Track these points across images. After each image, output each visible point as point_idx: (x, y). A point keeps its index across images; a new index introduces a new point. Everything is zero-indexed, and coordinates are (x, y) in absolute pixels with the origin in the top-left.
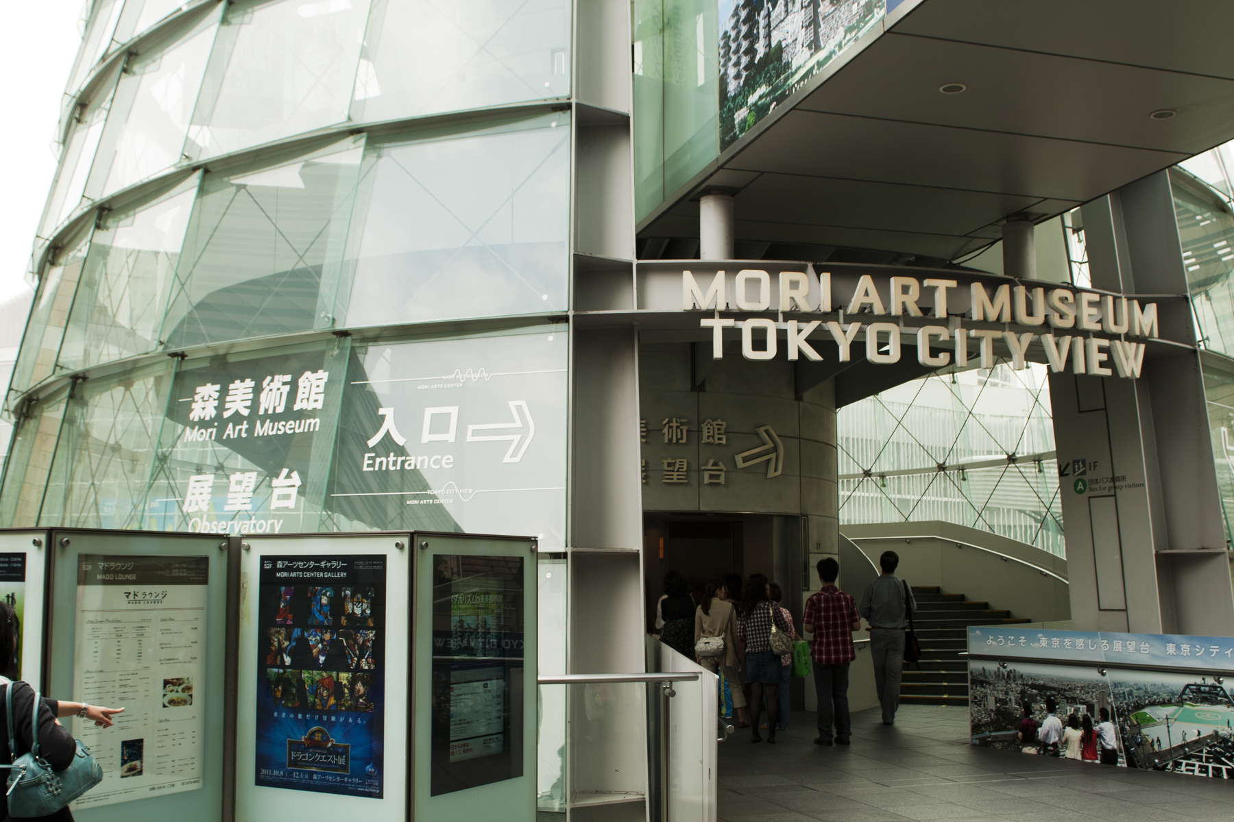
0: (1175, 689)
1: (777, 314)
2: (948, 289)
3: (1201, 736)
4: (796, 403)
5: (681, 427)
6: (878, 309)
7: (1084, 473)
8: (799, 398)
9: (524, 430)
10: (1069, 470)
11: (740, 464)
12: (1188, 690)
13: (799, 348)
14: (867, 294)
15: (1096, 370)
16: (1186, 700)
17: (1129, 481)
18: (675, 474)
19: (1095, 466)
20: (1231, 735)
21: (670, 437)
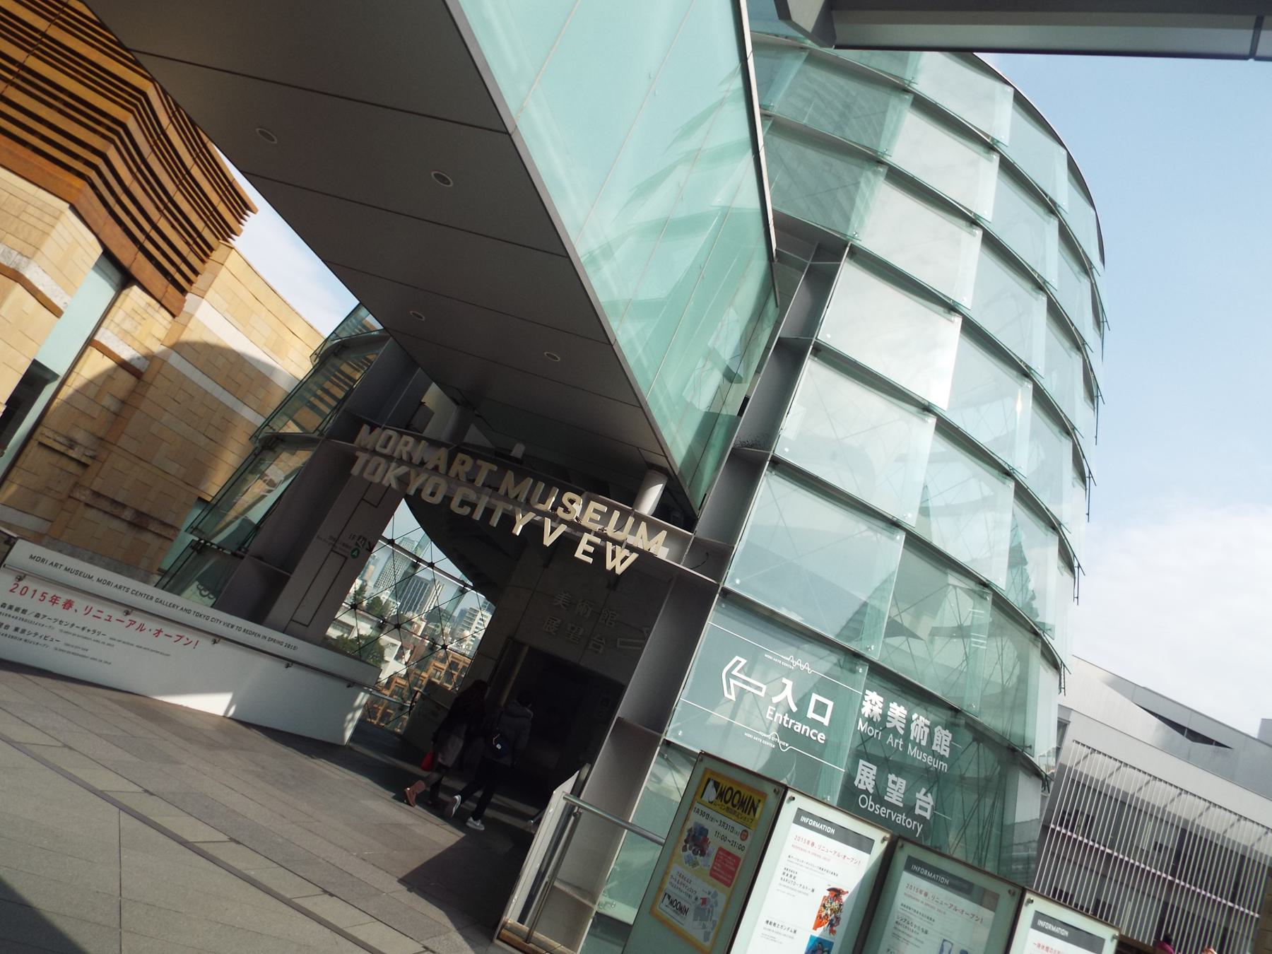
2: (490, 471)
9: (729, 675)
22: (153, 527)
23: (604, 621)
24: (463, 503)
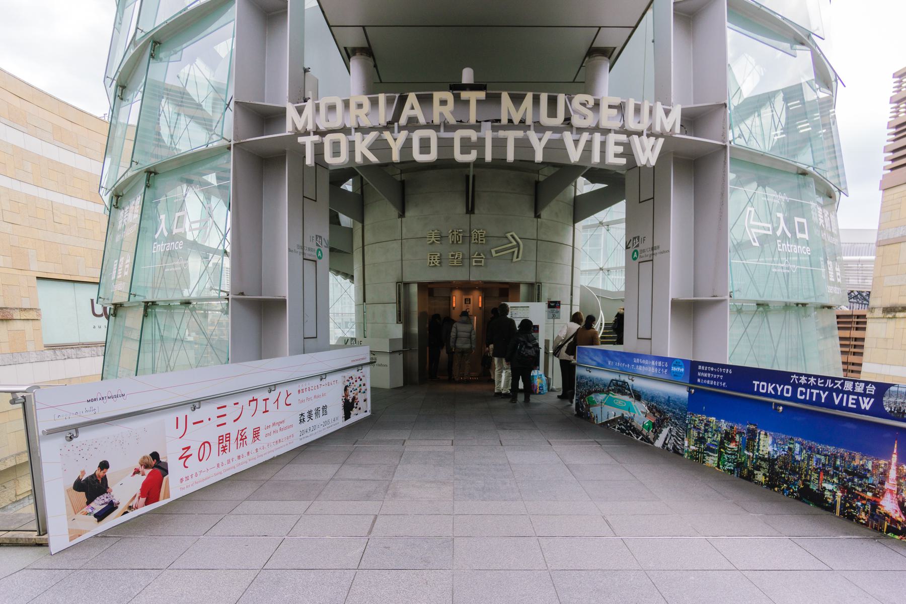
0: (606, 382)
1: (351, 129)
2: (479, 102)
3: (616, 417)
4: (535, 219)
5: (459, 234)
6: (422, 120)
7: (638, 246)
8: (537, 216)
10: (630, 245)
11: (494, 254)
12: (612, 384)
13: (361, 152)
14: (412, 108)
15: (611, 160)
16: (610, 390)
17: (661, 249)
18: (455, 260)
19: (644, 240)
20: (630, 418)
21: (453, 240)
22: (17, 315)
23: (476, 241)
24: (466, 149)
